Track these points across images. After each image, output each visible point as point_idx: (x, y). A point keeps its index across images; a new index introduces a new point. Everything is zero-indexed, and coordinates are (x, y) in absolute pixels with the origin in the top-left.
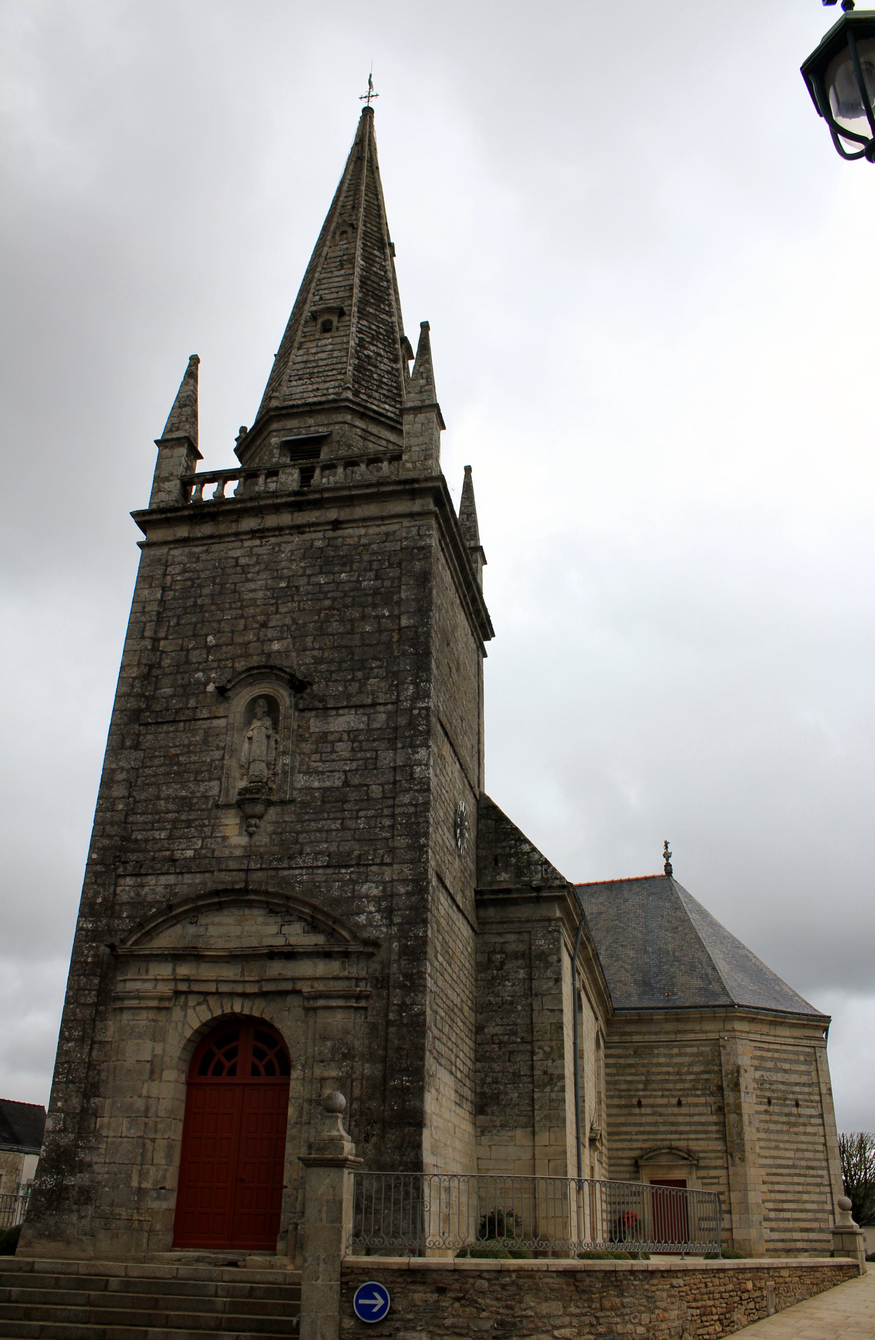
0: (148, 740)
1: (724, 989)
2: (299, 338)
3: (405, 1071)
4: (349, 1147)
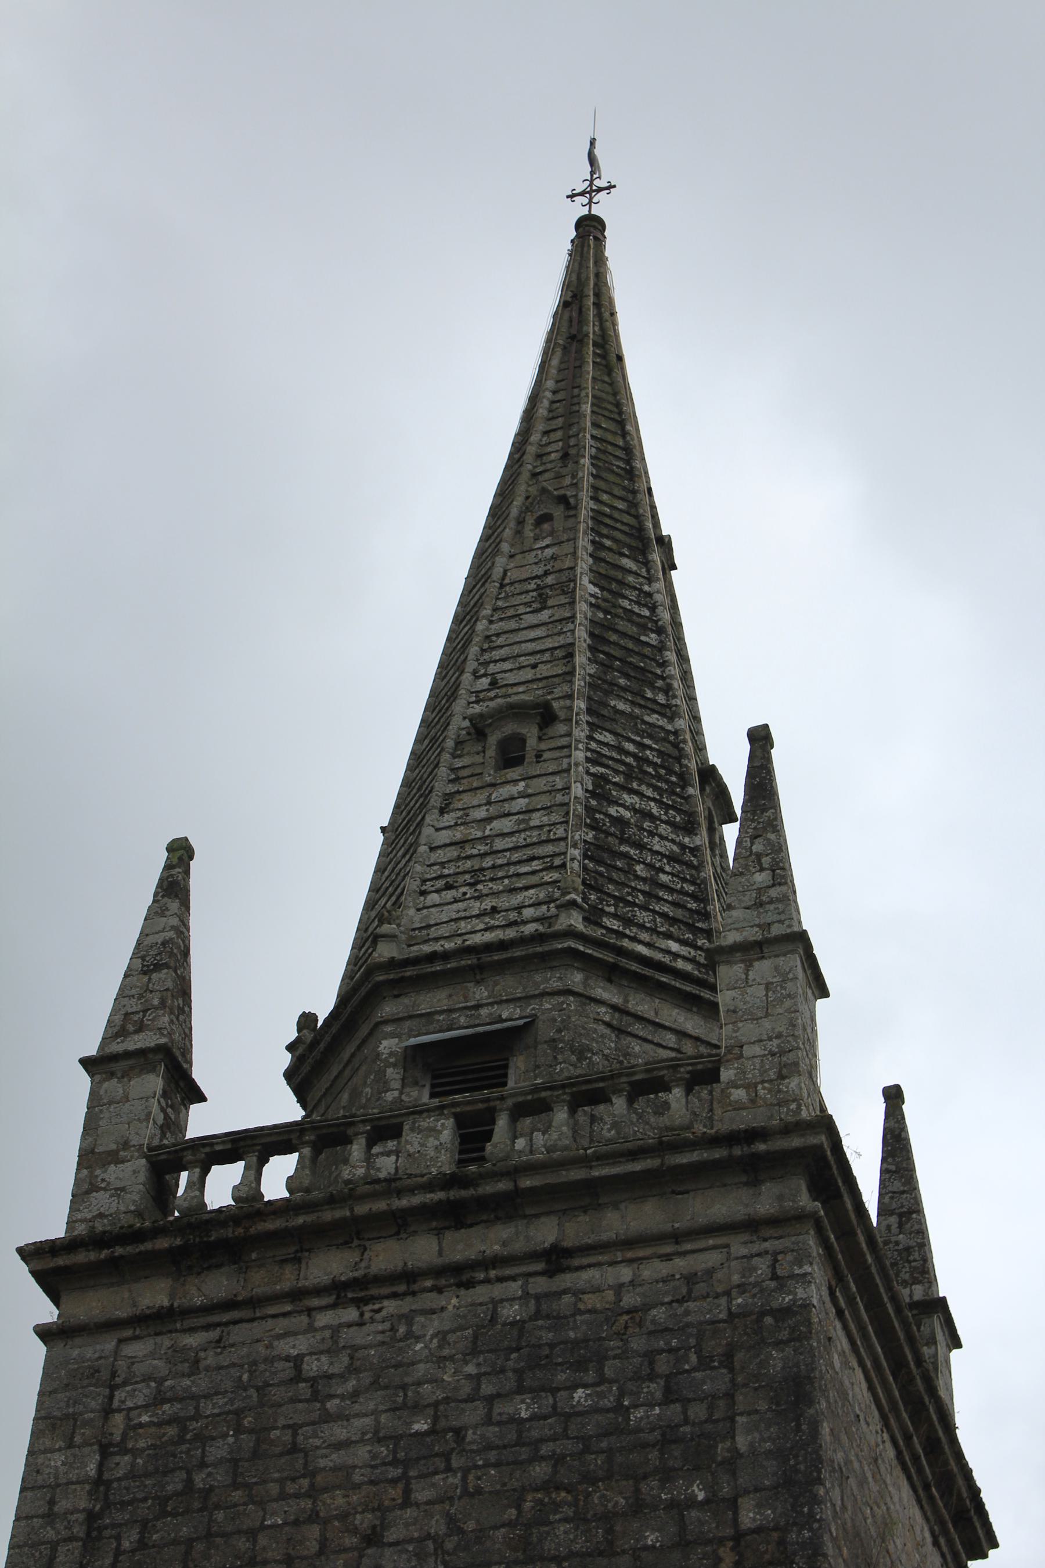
2: (441, 786)
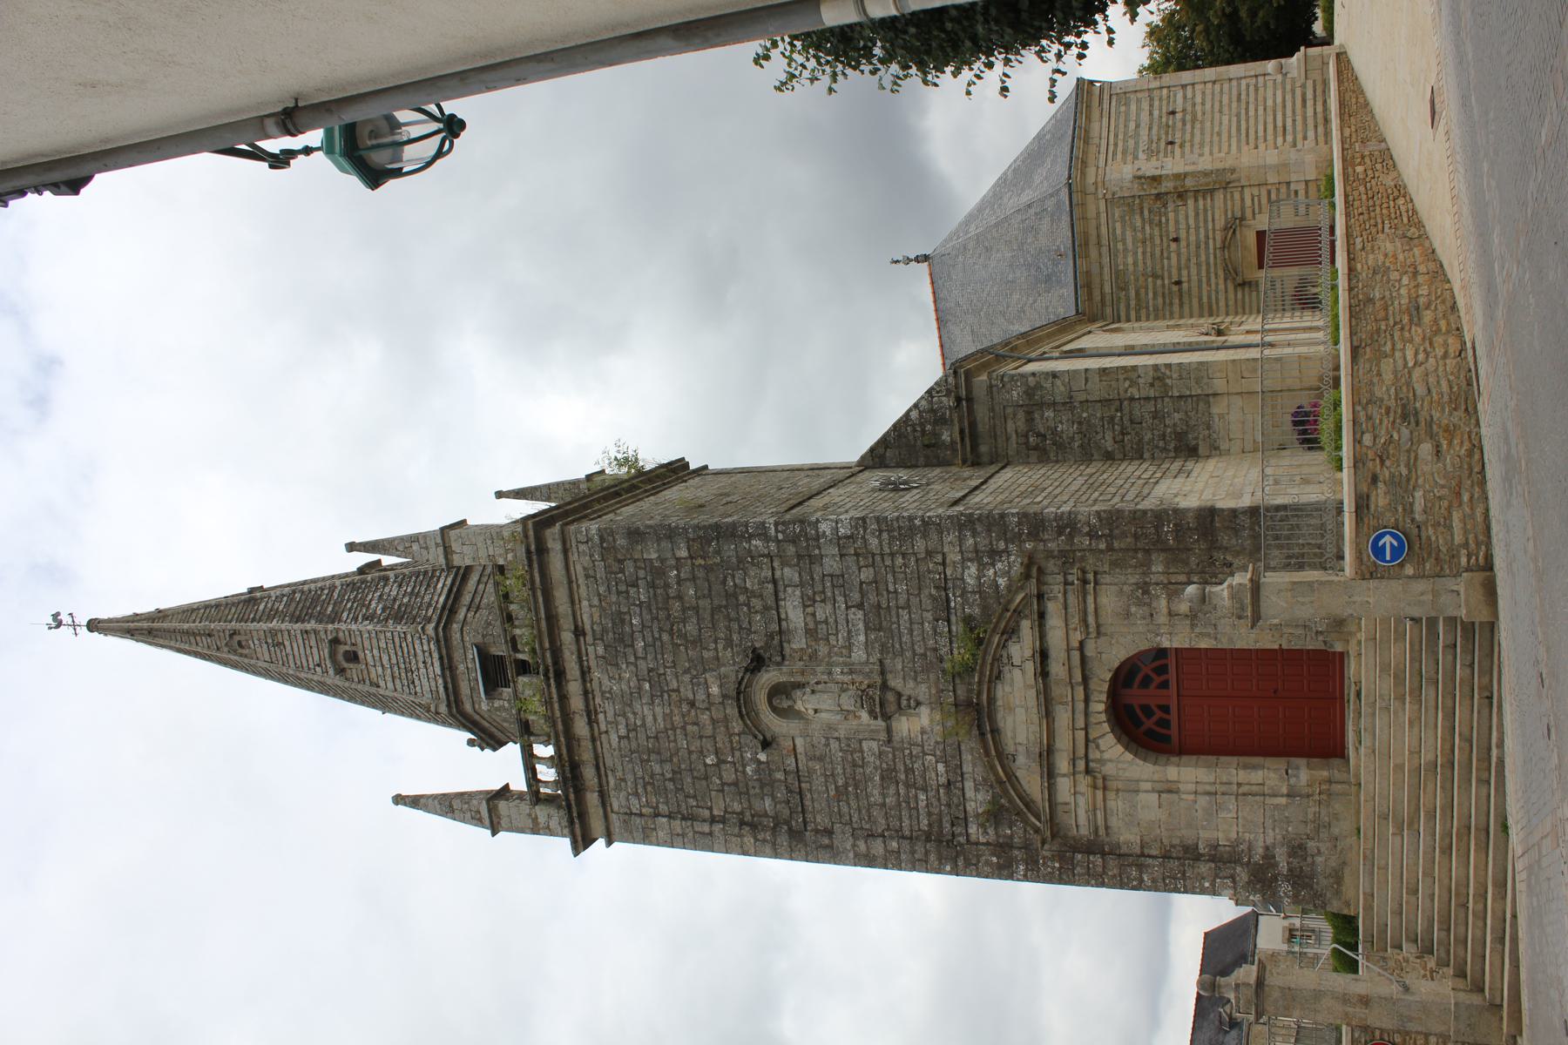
0: (822, 820)
1: (1052, 195)
2: (367, 688)
3: (1158, 528)
4: (1241, 579)
